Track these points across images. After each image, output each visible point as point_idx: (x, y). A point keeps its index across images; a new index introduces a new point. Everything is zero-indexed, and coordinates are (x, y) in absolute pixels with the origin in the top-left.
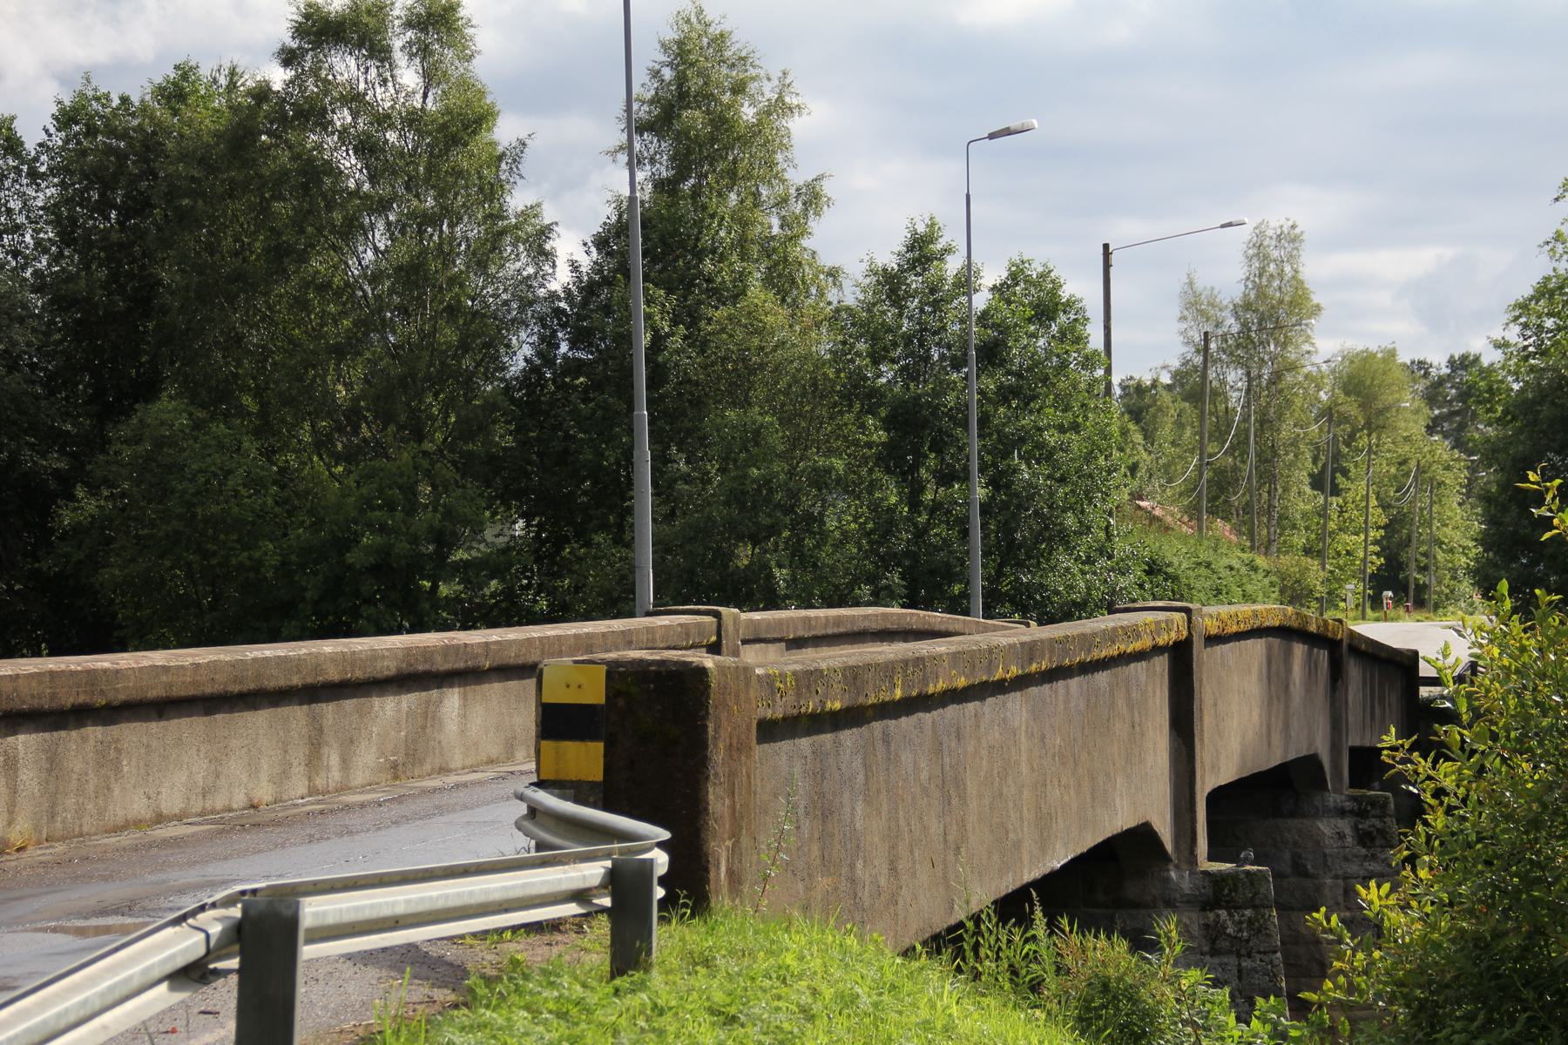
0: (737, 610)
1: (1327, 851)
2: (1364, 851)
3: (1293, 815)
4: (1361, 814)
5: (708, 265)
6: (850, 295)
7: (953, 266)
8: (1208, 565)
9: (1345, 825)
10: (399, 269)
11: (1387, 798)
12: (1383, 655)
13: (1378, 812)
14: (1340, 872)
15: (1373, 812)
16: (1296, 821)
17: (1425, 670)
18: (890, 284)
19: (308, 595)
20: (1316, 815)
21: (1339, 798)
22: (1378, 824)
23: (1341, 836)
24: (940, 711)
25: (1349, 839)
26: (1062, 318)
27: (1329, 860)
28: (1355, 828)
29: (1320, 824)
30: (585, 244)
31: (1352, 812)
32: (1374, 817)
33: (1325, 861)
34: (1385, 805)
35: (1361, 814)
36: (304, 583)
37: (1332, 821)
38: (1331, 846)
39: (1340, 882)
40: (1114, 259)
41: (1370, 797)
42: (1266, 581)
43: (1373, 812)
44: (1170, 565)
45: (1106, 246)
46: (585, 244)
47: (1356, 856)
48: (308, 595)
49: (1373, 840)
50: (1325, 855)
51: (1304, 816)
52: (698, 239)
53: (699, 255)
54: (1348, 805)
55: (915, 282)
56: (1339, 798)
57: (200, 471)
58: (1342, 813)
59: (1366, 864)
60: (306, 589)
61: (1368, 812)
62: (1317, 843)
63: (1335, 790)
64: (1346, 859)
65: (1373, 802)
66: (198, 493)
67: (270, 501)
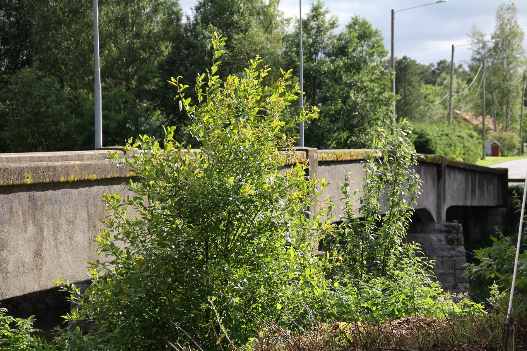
0: (316, 149)
1: (435, 247)
2: (449, 247)
3: (421, 232)
4: (449, 232)
5: (236, 17)
6: (291, 29)
7: (328, 18)
8: (447, 135)
9: (442, 236)
10: (117, 19)
11: (459, 226)
12: (479, 170)
13: (455, 231)
14: (440, 255)
15: (454, 231)
16: (422, 234)
17: (510, 177)
18: (305, 25)
19: (78, 143)
20: (430, 232)
21: (439, 226)
22: (456, 236)
23: (440, 241)
24: (87, 188)
25: (444, 242)
26: (373, 39)
27: (435, 250)
28: (446, 238)
29: (432, 236)
30: (192, 9)
31: (445, 231)
32: (454, 233)
33: (434, 251)
34: (458, 229)
35: (449, 232)
36: (77, 138)
37: (437, 235)
38: (436, 244)
39: (440, 258)
40: (395, 16)
41: (452, 225)
42: (477, 142)
43: (454, 231)
44: (428, 135)
45: (392, 11)
46: (192, 9)
47: (446, 248)
48: (78, 143)
49: (453, 242)
50: (434, 248)
51: (425, 233)
52: (232, 8)
53: (232, 14)
54: (443, 228)
55: (313, 24)
56: (439, 226)
57: (38, 95)
58: (441, 231)
59: (450, 252)
60: (77, 141)
61: (451, 231)
62: (431, 243)
63: (438, 223)
64: (442, 249)
65: (454, 228)
66: (36, 104)
67: (64, 107)
